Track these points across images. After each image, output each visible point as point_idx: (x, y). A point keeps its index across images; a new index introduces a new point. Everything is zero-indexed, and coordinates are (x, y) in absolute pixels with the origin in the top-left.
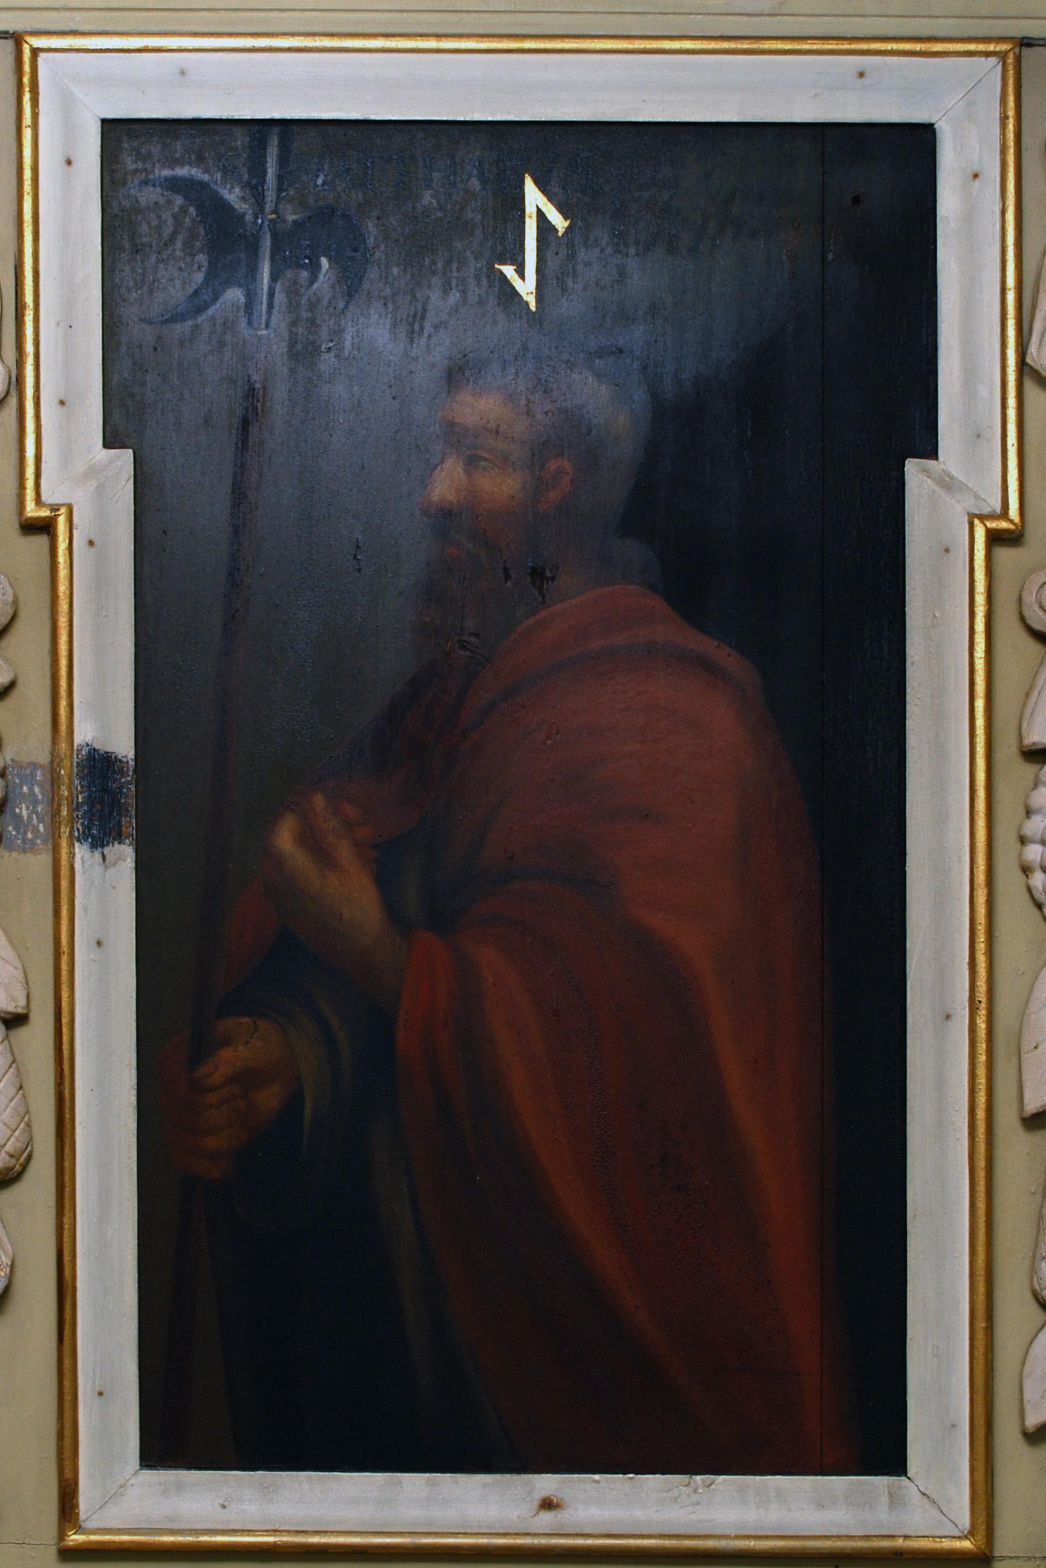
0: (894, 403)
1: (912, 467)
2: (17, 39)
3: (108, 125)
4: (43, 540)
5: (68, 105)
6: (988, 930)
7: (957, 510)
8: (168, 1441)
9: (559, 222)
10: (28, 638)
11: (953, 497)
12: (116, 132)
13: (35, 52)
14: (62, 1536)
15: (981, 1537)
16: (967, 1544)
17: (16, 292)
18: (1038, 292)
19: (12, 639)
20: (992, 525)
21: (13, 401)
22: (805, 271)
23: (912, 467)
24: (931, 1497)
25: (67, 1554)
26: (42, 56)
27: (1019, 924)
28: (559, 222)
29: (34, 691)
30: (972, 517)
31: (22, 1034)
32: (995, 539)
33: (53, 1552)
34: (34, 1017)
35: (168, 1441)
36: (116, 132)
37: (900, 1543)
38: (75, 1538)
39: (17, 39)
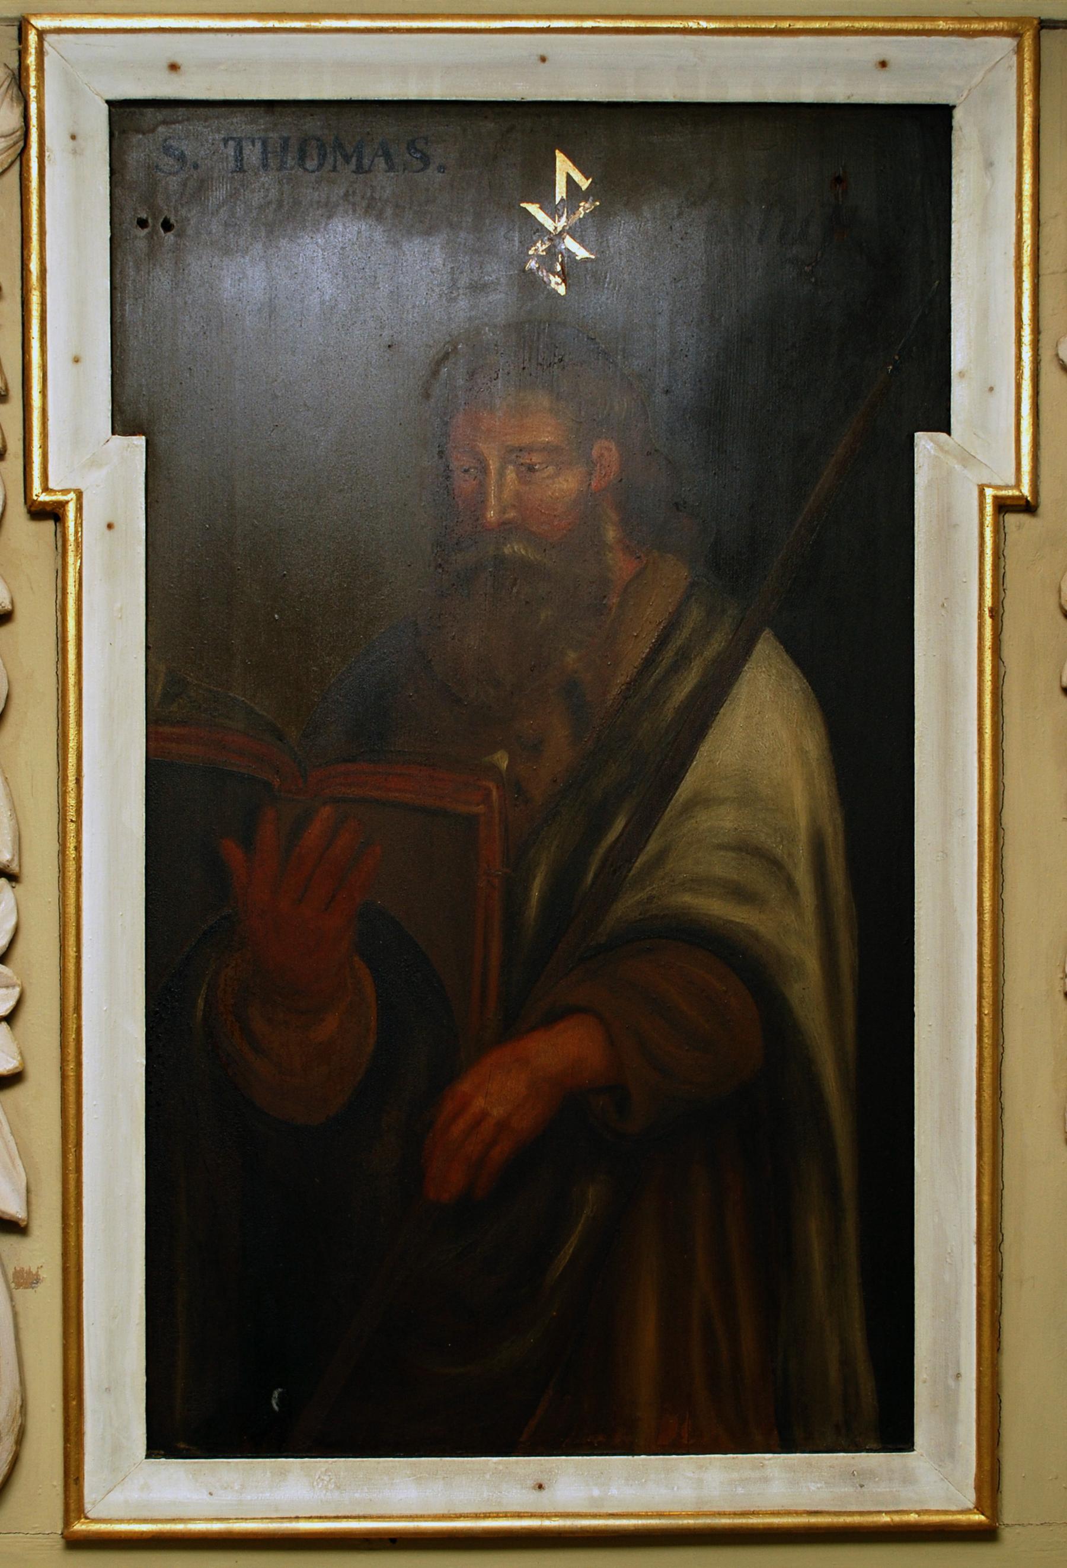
1: (925, 443)
8: (174, 1432)
9: (584, 184)
11: (956, 475)
13: (41, 34)
14: (67, 1522)
16: (979, 1518)
17: (23, 316)
22: (835, 233)
23: (925, 443)
25: (76, 1543)
26: (49, 38)
28: (584, 184)
29: (40, 951)
33: (59, 1542)
34: (33, 1074)
35: (174, 1432)
37: (913, 1518)
38: (79, 1527)
39: (22, 26)
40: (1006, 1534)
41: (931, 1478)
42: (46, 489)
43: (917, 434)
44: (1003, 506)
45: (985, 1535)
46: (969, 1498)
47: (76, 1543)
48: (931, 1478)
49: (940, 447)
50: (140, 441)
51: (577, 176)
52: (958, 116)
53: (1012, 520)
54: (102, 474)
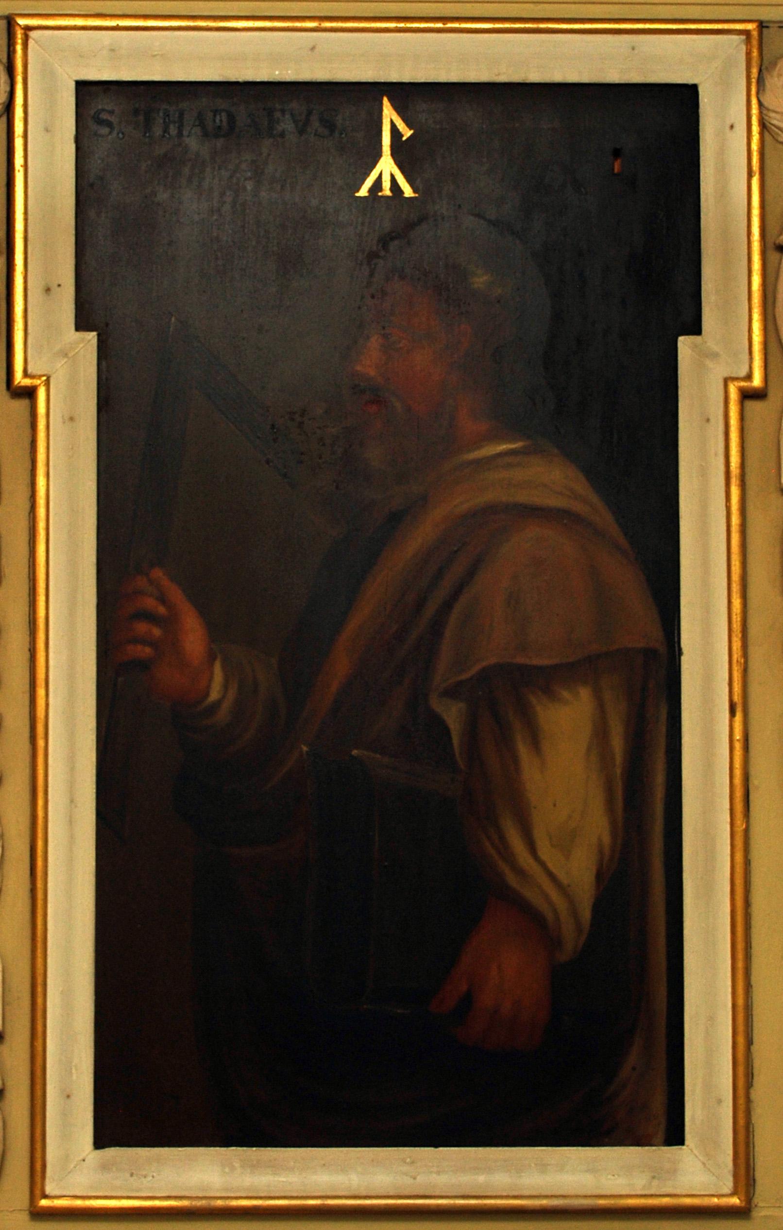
1: (684, 343)
5: (48, 73)
8: (121, 1120)
11: (711, 369)
13: (28, 29)
16: (735, 1201)
23: (684, 343)
25: (39, 1215)
30: (726, 381)
35: (121, 1120)
38: (44, 1203)
39: (10, 22)
40: (755, 1214)
41: (696, 1170)
42: (26, 374)
43: (681, 339)
44: (747, 395)
45: (742, 1213)
46: (728, 1185)
47: (39, 1215)
48: (696, 1170)
49: (695, 346)
50: (92, 336)
51: (401, 126)
52: (701, 90)
53: (750, 404)
54: (59, 359)
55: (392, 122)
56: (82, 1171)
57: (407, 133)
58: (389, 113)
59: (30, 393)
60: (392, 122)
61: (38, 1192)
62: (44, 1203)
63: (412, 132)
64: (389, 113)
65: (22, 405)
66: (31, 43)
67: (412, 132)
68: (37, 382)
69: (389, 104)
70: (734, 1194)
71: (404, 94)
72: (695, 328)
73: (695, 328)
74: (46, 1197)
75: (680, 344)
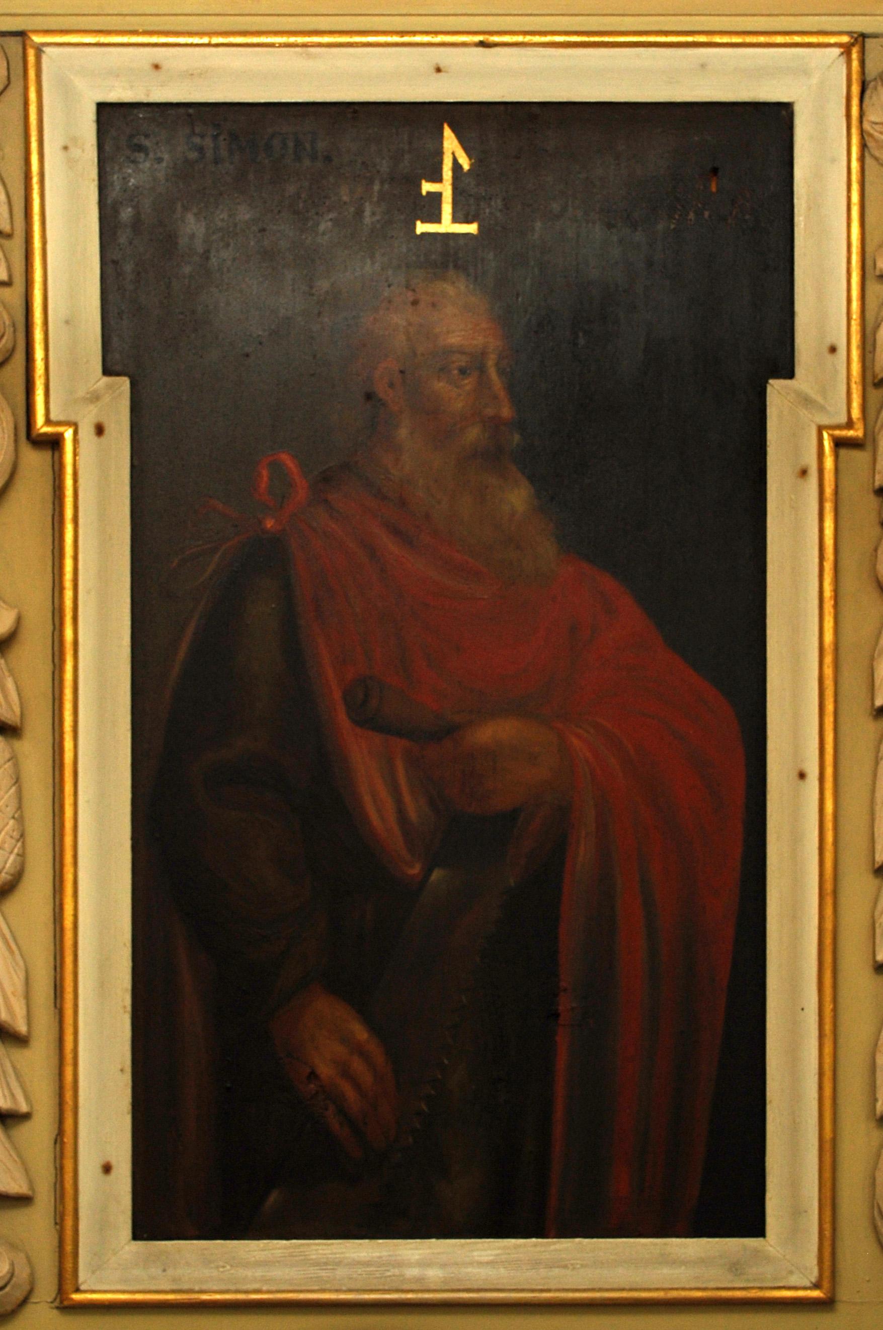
0: (760, 339)
1: (776, 388)
2: (22, 34)
3: (102, 107)
4: (47, 50)
5: (67, 90)
6: (831, 893)
7: (811, 419)
8: (155, 1217)
10: (32, 652)
11: (807, 413)
12: (109, 114)
15: (826, 1284)
16: (816, 1294)
18: (877, 1164)
19: (13, 904)
20: (837, 433)
21: (19, 357)
23: (776, 388)
24: (784, 1253)
27: (860, 887)
30: (820, 429)
31: (23, 1131)
32: (839, 444)
35: (155, 1217)
36: (109, 114)
38: (76, 1297)
40: (841, 1307)
42: (48, 422)
45: (827, 1304)
47: (68, 1308)
53: (843, 452)
55: (455, 161)
56: (117, 1263)
57: (465, 163)
58: (450, 143)
59: (54, 443)
60: (455, 161)
61: (69, 1286)
62: (76, 1297)
63: (424, 193)
64: (450, 143)
65: (35, 461)
66: (45, 59)
67: (424, 193)
68: (60, 429)
69: (452, 135)
70: (817, 1286)
71: (468, 117)
72: (789, 373)
73: (789, 373)
74: (77, 1290)
75: (769, 389)
